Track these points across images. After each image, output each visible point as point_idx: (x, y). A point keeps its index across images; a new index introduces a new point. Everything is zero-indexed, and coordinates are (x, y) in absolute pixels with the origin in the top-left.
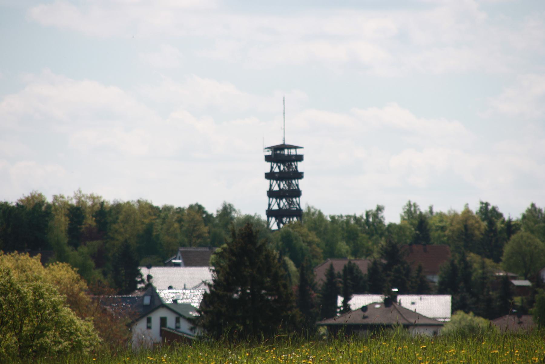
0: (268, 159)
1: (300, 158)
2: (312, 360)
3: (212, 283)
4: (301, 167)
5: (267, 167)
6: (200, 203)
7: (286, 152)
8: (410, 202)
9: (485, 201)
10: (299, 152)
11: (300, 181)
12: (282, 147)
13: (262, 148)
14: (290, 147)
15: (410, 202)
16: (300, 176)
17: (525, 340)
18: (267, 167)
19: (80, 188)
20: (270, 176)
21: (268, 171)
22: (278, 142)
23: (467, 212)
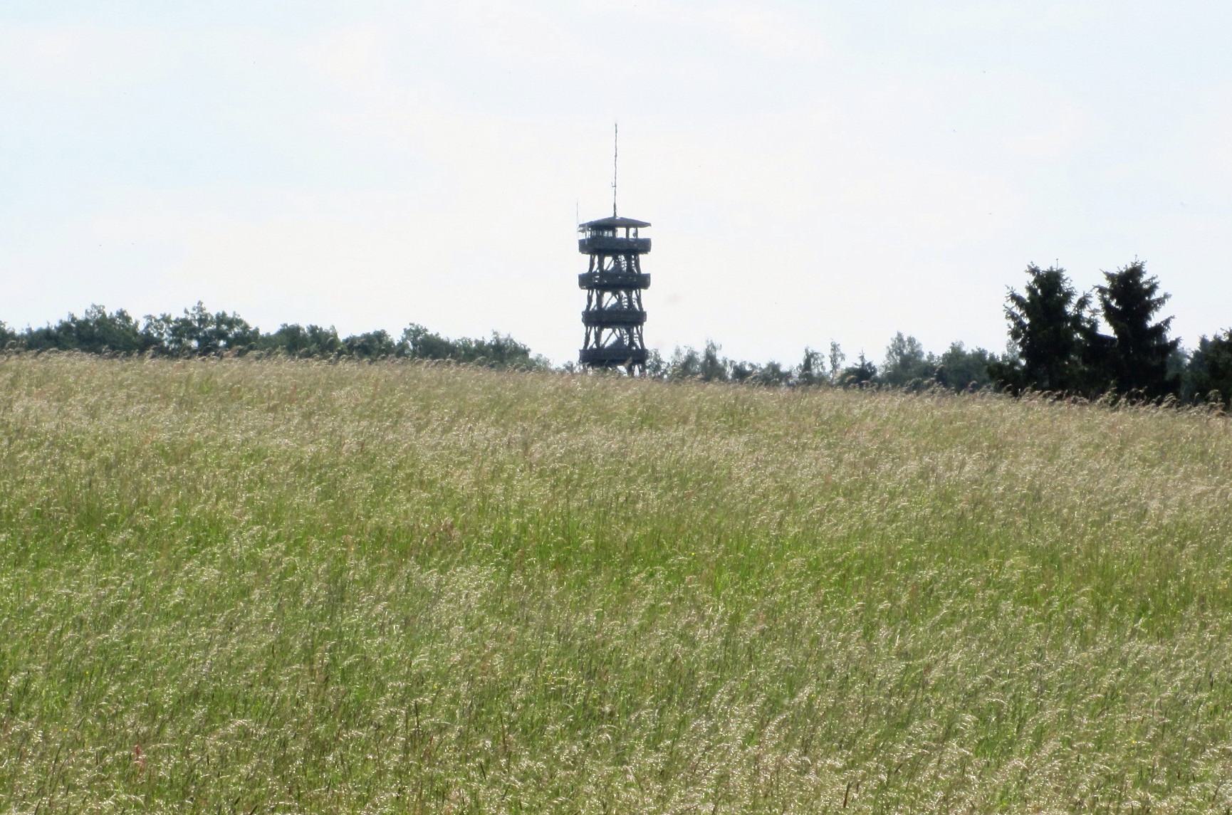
0: (585, 247)
1: (644, 246)
2: (155, 715)
3: (1025, 295)
4: (646, 264)
5: (583, 263)
6: (291, 323)
7: (621, 233)
8: (899, 335)
9: (1044, 268)
10: (643, 234)
11: (643, 291)
12: (611, 225)
13: (576, 228)
14: (628, 224)
15: (899, 335)
16: (643, 281)
17: (759, 782)
18: (583, 263)
19: (200, 303)
20: (586, 281)
21: (586, 270)
22: (604, 214)
23: (256, 331)
